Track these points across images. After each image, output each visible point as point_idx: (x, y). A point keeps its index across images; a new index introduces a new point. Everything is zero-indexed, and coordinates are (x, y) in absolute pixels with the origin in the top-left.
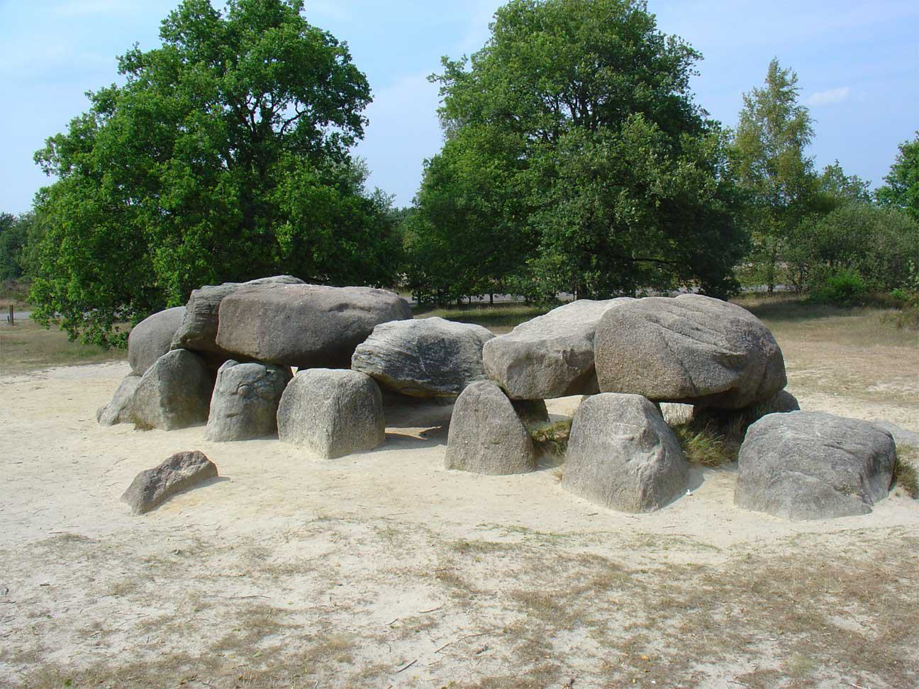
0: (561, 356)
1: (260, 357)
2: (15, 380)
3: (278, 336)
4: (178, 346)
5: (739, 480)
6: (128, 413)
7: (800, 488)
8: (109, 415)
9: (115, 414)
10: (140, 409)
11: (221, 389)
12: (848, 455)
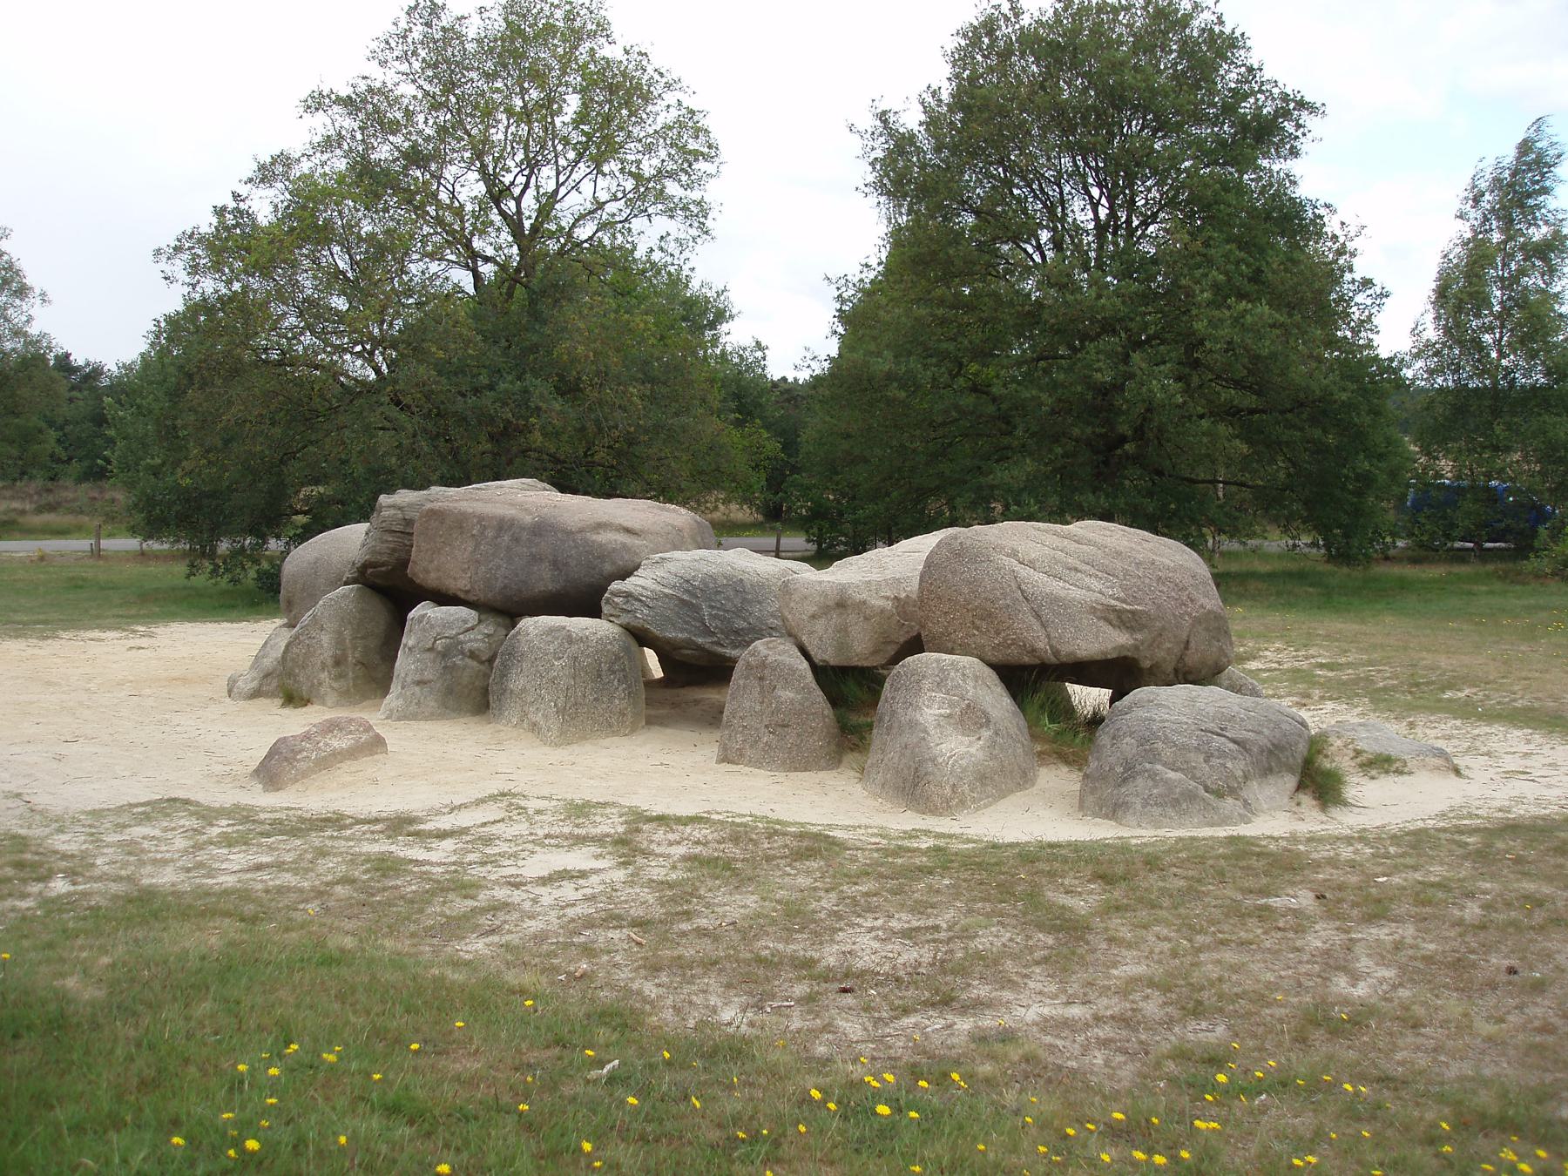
0: (889, 605)
1: (471, 598)
2: (103, 635)
3: (499, 567)
4: (354, 581)
5: (1086, 776)
6: (275, 683)
7: (1156, 786)
8: (246, 685)
9: (255, 684)
10: (290, 675)
11: (411, 643)
12: (1231, 745)
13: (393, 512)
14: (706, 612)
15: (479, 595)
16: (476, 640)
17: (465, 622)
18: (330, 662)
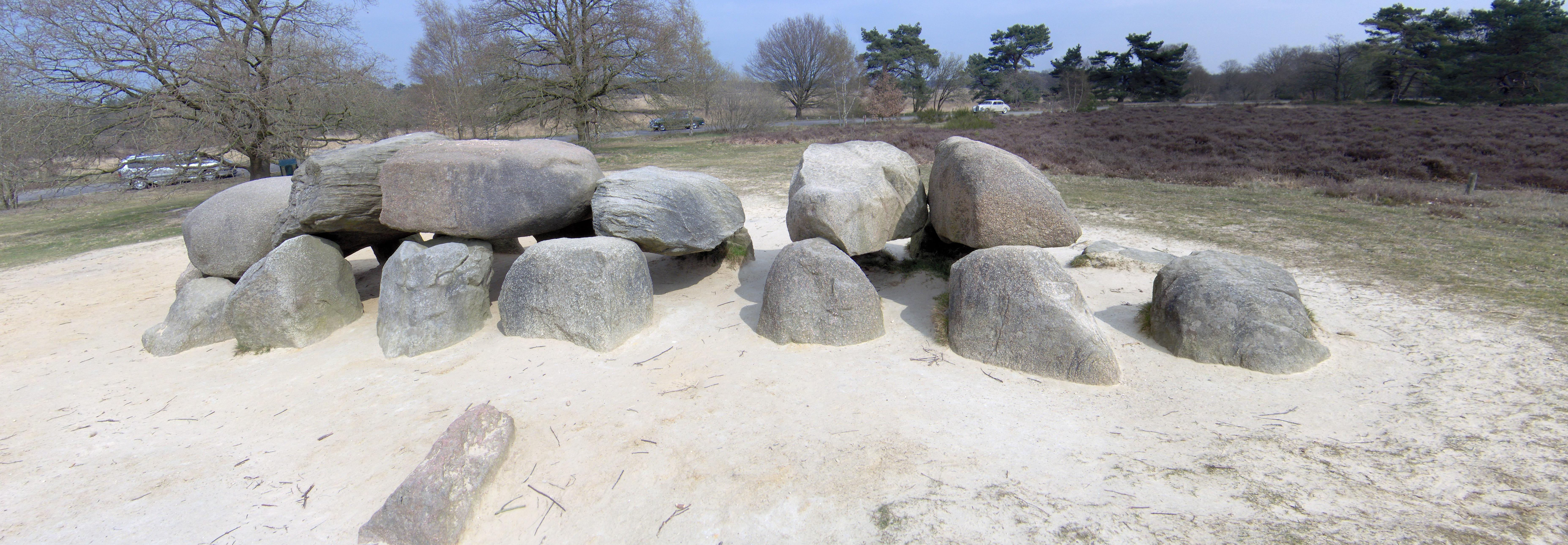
13: (333, 170)
14: (684, 218)
15: (471, 231)
16: (472, 268)
17: (460, 255)
18: (291, 309)
